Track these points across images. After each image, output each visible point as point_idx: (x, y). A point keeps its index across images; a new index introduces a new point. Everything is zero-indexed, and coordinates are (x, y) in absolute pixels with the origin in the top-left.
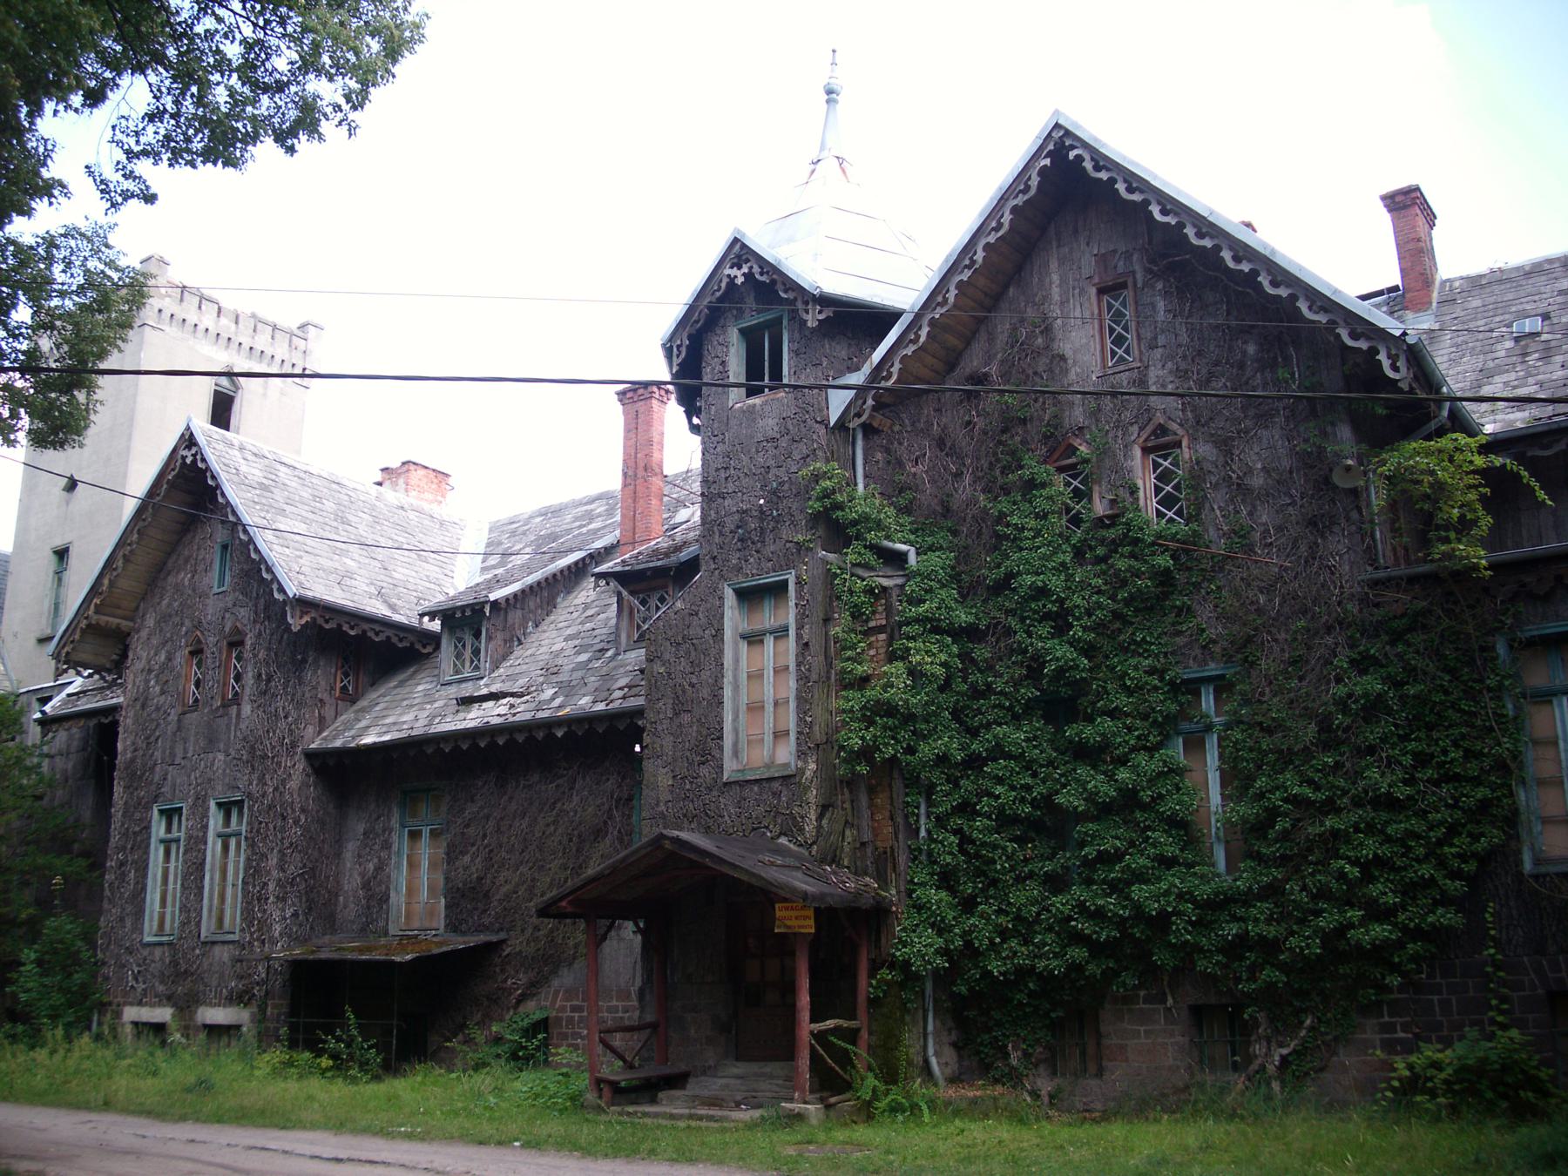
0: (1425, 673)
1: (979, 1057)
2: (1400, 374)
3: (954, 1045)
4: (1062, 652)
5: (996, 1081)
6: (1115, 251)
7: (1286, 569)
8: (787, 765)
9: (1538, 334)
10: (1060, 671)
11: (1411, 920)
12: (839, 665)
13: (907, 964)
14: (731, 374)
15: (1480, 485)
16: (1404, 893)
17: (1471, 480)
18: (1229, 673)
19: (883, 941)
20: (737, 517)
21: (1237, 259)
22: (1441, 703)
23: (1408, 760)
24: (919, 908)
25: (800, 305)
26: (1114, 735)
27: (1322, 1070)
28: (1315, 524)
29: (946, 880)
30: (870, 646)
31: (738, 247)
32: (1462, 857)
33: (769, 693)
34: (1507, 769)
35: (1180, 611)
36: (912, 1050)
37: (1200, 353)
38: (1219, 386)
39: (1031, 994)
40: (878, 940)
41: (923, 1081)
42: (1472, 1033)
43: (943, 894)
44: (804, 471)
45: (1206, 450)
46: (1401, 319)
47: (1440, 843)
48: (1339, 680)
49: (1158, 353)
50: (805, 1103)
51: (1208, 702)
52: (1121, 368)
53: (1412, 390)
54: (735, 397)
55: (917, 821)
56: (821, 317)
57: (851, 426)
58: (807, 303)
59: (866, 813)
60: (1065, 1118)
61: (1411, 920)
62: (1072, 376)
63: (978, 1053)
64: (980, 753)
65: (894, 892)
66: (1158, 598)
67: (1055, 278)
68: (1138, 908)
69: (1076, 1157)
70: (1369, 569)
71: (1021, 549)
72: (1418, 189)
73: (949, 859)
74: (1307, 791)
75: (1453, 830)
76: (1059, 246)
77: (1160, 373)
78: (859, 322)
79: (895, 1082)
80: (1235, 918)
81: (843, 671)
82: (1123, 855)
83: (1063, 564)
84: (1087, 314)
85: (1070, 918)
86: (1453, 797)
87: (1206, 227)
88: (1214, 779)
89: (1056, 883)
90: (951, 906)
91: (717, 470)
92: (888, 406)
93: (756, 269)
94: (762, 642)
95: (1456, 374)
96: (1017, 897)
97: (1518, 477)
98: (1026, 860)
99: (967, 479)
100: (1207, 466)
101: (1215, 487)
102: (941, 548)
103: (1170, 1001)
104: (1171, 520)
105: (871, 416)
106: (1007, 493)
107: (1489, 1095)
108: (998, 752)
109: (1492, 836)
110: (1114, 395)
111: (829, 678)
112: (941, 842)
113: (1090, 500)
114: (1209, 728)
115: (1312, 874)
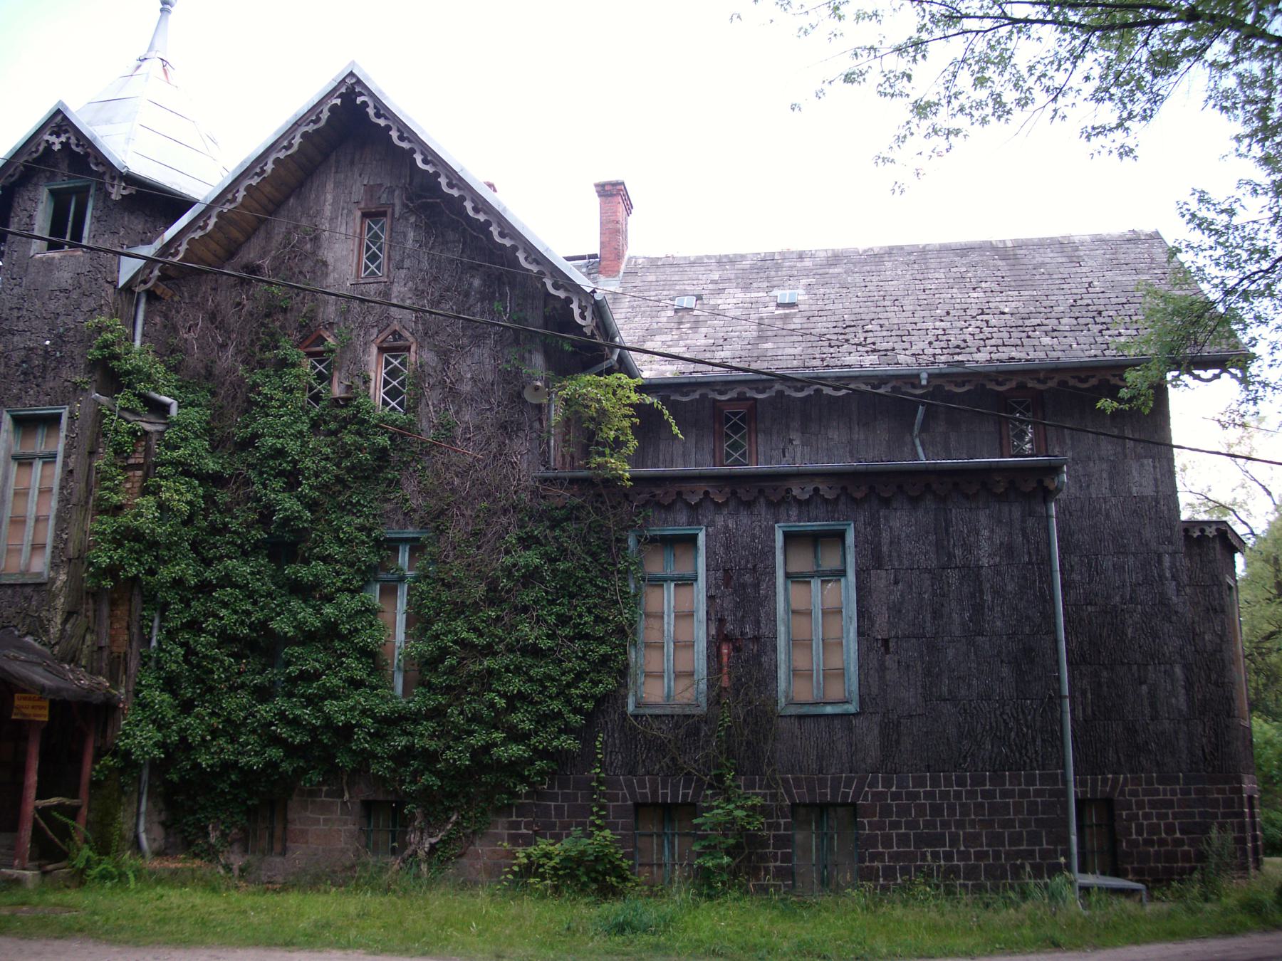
0: (573, 554)
1: (183, 835)
2: (587, 322)
3: (163, 824)
4: (290, 504)
5: (196, 855)
6: (381, 185)
7: (479, 460)
8: (40, 574)
9: (692, 309)
10: (286, 520)
11: (540, 743)
12: (98, 492)
13: (128, 753)
14: (36, 227)
15: (633, 416)
16: (538, 722)
17: (627, 411)
18: (423, 536)
19: (109, 731)
20: (23, 353)
21: (476, 210)
22: (582, 578)
23: (552, 620)
24: (144, 706)
25: (107, 179)
26: (325, 577)
27: (461, 856)
28: (506, 428)
29: (170, 684)
30: (127, 480)
31: (59, 118)
32: (584, 698)
33: (31, 510)
34: (624, 633)
35: (391, 481)
36: (125, 827)
37: (436, 279)
38: (447, 307)
39: (233, 784)
40: (105, 731)
41: (133, 854)
42: (577, 831)
43: (166, 696)
44: (90, 323)
45: (429, 357)
46: (594, 281)
47: (569, 685)
48: (507, 552)
49: (403, 273)
50: (24, 869)
51: (403, 558)
52: (371, 280)
53: (593, 336)
54: (37, 249)
55: (150, 632)
56: (125, 193)
57: (137, 290)
58: (113, 178)
59: (106, 622)
60: (252, 888)
61: (540, 743)
62: (330, 280)
63: (183, 831)
64: (211, 581)
65: (123, 691)
66: (374, 470)
67: (329, 197)
68: (328, 719)
69: (256, 920)
70: (542, 468)
71: (267, 415)
72: (623, 184)
73: (174, 667)
74: (473, 636)
75: (579, 676)
76: (336, 172)
77: (402, 289)
78: (158, 203)
79: (107, 854)
80: (405, 733)
81: (101, 499)
82: (321, 675)
83: (301, 432)
84: (350, 232)
85: (272, 724)
86: (582, 651)
87: (456, 180)
88: (401, 620)
89: (263, 694)
90: (172, 707)
91: (11, 309)
92: (170, 278)
93: (73, 141)
94: (31, 464)
95: (627, 329)
96: (229, 703)
97: (661, 413)
98: (240, 673)
99: (231, 350)
100: (428, 370)
101: (432, 387)
102: (200, 405)
103: (347, 796)
104: (393, 409)
105: (155, 285)
106: (263, 367)
107: (584, 879)
108: (227, 580)
109: (608, 683)
110: (362, 301)
111: (87, 503)
112: (169, 652)
113: (330, 383)
114: (402, 579)
115: (469, 702)
